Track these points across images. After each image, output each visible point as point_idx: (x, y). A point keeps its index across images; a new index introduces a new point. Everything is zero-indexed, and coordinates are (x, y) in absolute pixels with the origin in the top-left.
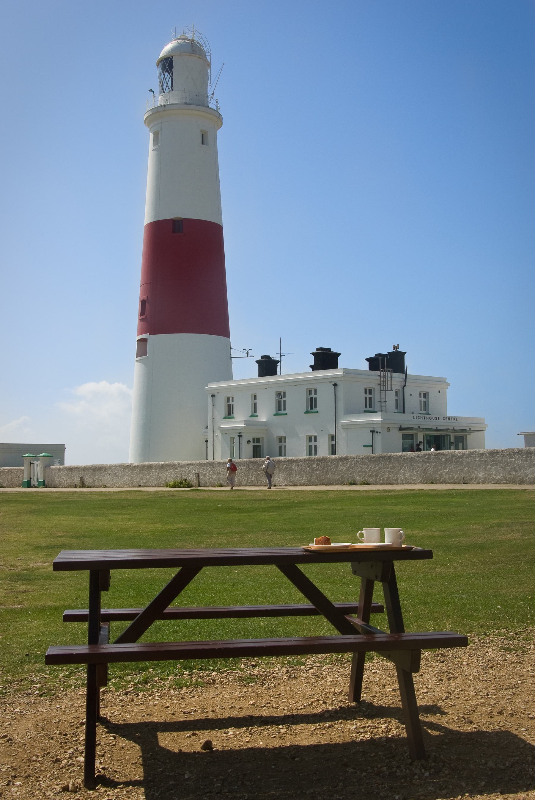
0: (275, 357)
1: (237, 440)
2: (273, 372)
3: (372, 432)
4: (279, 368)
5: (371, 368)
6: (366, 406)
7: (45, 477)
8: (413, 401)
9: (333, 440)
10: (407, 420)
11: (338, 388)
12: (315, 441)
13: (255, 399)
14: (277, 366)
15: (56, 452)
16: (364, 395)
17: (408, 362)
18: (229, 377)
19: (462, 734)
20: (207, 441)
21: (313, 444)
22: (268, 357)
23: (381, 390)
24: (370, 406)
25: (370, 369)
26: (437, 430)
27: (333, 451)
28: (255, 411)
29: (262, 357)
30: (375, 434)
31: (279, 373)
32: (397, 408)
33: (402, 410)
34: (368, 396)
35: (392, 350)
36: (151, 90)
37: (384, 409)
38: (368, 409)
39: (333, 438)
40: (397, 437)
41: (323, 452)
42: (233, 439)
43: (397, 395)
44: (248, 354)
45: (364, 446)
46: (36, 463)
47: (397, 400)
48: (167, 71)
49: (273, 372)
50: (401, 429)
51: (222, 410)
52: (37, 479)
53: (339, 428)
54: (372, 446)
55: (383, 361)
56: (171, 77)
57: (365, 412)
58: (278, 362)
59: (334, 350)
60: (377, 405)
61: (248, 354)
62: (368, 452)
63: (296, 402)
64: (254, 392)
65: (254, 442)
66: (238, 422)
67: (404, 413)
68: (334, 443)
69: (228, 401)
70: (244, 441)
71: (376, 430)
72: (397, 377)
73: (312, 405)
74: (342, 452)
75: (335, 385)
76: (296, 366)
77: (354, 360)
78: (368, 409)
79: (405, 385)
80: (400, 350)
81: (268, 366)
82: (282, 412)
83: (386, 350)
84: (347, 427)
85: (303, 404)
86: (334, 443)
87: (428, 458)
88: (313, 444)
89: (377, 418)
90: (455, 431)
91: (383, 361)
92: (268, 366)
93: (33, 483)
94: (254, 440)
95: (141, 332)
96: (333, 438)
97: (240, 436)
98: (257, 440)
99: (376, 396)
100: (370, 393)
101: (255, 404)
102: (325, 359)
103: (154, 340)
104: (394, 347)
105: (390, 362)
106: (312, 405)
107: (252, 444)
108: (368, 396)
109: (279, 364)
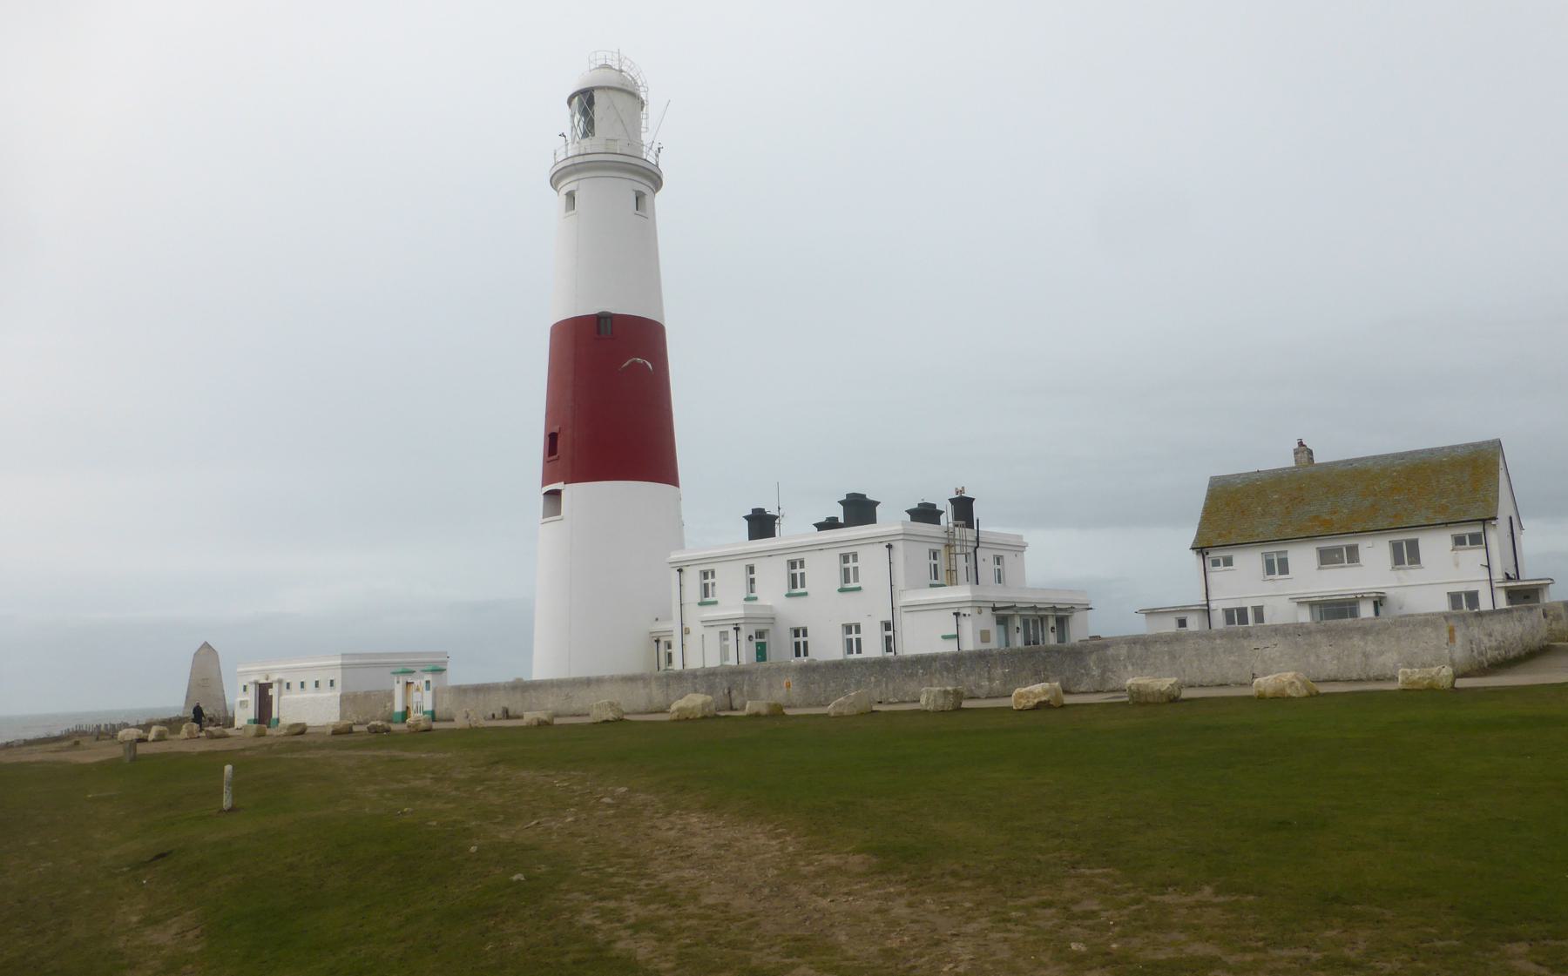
0: (771, 510)
1: (732, 633)
2: (770, 533)
3: (957, 614)
7: (434, 704)
8: (987, 569)
15: (1062, 618)
17: (978, 511)
18: (681, 547)
19: (83, 771)
21: (854, 636)
22: (762, 510)
26: (1034, 608)
27: (889, 643)
30: (961, 619)
35: (954, 496)
39: (887, 626)
40: (988, 621)
45: (944, 637)
49: (770, 533)
50: (994, 609)
54: (957, 637)
58: (775, 517)
62: (951, 647)
63: (822, 572)
64: (750, 562)
66: (730, 604)
70: (743, 636)
71: (962, 611)
72: (970, 534)
73: (302, 684)
75: (890, 547)
80: (967, 494)
82: (799, 590)
84: (912, 608)
88: (854, 636)
89: (962, 592)
90: (1054, 609)
92: (762, 525)
95: (546, 480)
97: (737, 629)
98: (760, 634)
99: (942, 563)
101: (752, 581)
102: (859, 509)
103: (573, 493)
106: (302, 684)
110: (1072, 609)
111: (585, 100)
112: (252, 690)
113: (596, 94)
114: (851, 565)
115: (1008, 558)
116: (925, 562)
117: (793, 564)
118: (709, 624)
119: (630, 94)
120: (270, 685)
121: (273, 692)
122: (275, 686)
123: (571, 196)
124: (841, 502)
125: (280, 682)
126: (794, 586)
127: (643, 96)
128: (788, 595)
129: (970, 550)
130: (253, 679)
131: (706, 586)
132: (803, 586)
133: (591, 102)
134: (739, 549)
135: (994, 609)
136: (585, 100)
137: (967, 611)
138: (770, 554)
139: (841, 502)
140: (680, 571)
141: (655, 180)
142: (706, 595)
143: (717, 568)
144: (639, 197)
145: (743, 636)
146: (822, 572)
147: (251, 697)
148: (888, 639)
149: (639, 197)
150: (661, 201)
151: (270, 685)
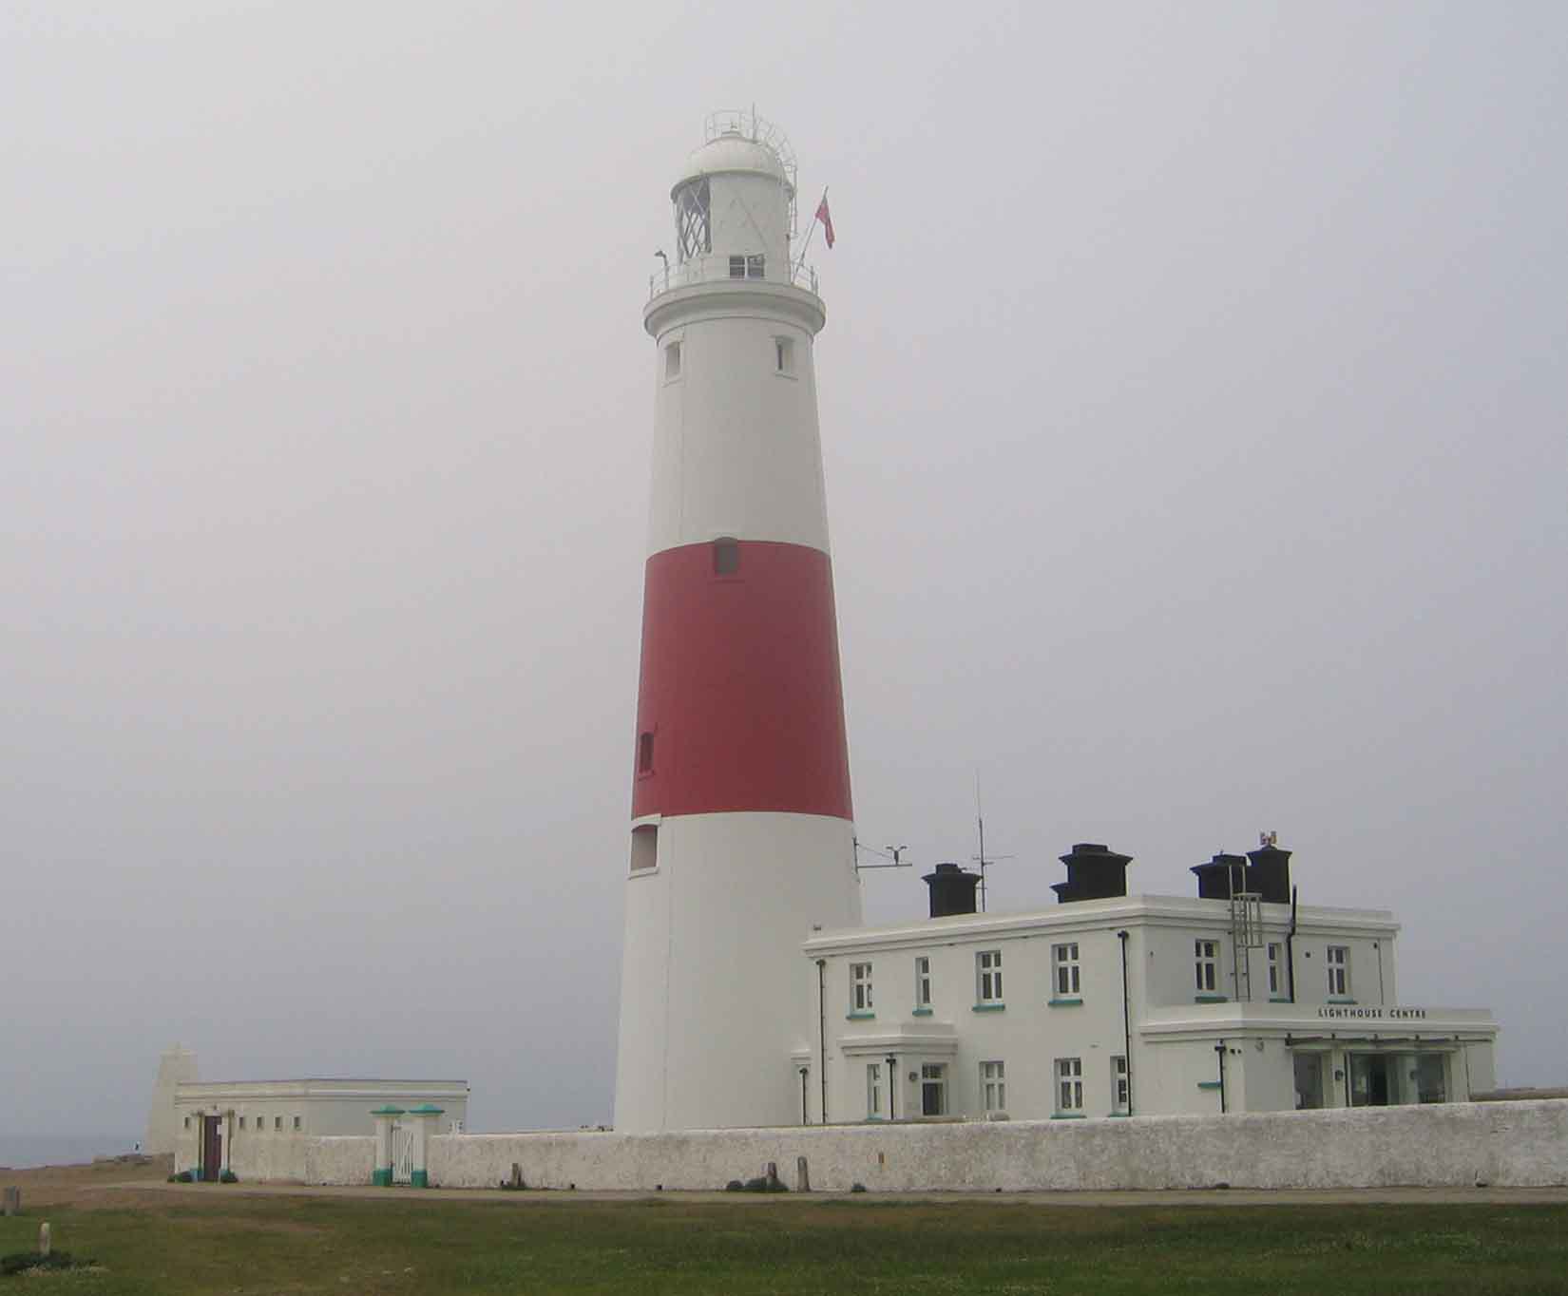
0: (969, 866)
1: (884, 1069)
3: (1221, 1050)
4: (978, 894)
5: (1204, 893)
6: (1200, 986)
8: (1312, 970)
9: (1121, 1070)
10: (1307, 1017)
11: (1132, 942)
12: (1078, 1072)
13: (926, 969)
14: (974, 889)
16: (1195, 959)
17: (1297, 874)
20: (804, 1072)
23: (1235, 946)
24: (1341, 991)
25: (1202, 895)
26: (1376, 1041)
28: (927, 999)
29: (938, 867)
30: (1229, 1058)
31: (979, 907)
32: (1274, 988)
33: (1287, 996)
34: (1204, 960)
35: (1258, 847)
36: (660, 254)
37: (1243, 991)
38: (1206, 992)
39: (1122, 1064)
41: (1097, 1105)
42: (873, 1069)
43: (1272, 957)
44: (896, 857)
46: (405, 1127)
47: (1273, 969)
48: (696, 210)
51: (840, 998)
52: (408, 1166)
53: (1137, 1043)
54: (1221, 1085)
55: (1237, 874)
56: (706, 224)
57: (1200, 1000)
58: (977, 878)
59: (1116, 848)
60: (1223, 983)
61: (896, 857)
63: (1027, 973)
64: (921, 954)
65: (925, 1076)
66: (890, 1023)
67: (1292, 1000)
68: (1124, 1076)
69: (860, 975)
70: (900, 1074)
72: (1273, 913)
74: (1147, 1114)
75: (1124, 936)
76: (1021, 889)
77: (1161, 876)
78: (1206, 992)
79: (1290, 936)
80: (1279, 846)
81: (953, 891)
83: (1243, 844)
85: (1045, 984)
86: (1124, 1076)
87: (1384, 1124)
88: (1072, 1079)
89: (1228, 1015)
91: (1237, 874)
92: (953, 891)
93: (399, 1175)
94: (924, 1069)
95: (638, 812)
96: (1122, 1064)
97: (892, 1062)
98: (933, 1070)
100: (1209, 953)
101: (926, 982)
102: (1094, 872)
103: (675, 830)
104: (1263, 841)
105: (1261, 874)
107: (921, 1080)
108: (1204, 960)
109: (979, 884)
110: (1458, 1040)
111: (694, 194)
112: (195, 1123)
113: (714, 187)
114: (993, 970)
115: (1360, 956)
116: (1188, 961)
117: (1061, 952)
118: (852, 1051)
119: (768, 182)
120: (217, 1120)
121: (222, 1130)
122: (225, 1121)
123: (674, 351)
124: (1063, 859)
125: (231, 1114)
126: (987, 995)
127: (790, 178)
128: (1054, 1004)
129: (1281, 940)
130: (196, 1108)
131: (860, 988)
132: (1076, 988)
133: (705, 197)
134: (1183, 909)
135: (1289, 1041)
136: (694, 194)
137: (1237, 1046)
138: (951, 941)
139: (1123, 861)
140: (822, 964)
141: (810, 313)
142: (860, 1004)
143: (876, 961)
144: (783, 347)
145: (900, 1074)
146: (1027, 973)
147: (193, 1136)
148: (1122, 1085)
149: (783, 347)
150: (825, 350)
151: (217, 1120)
